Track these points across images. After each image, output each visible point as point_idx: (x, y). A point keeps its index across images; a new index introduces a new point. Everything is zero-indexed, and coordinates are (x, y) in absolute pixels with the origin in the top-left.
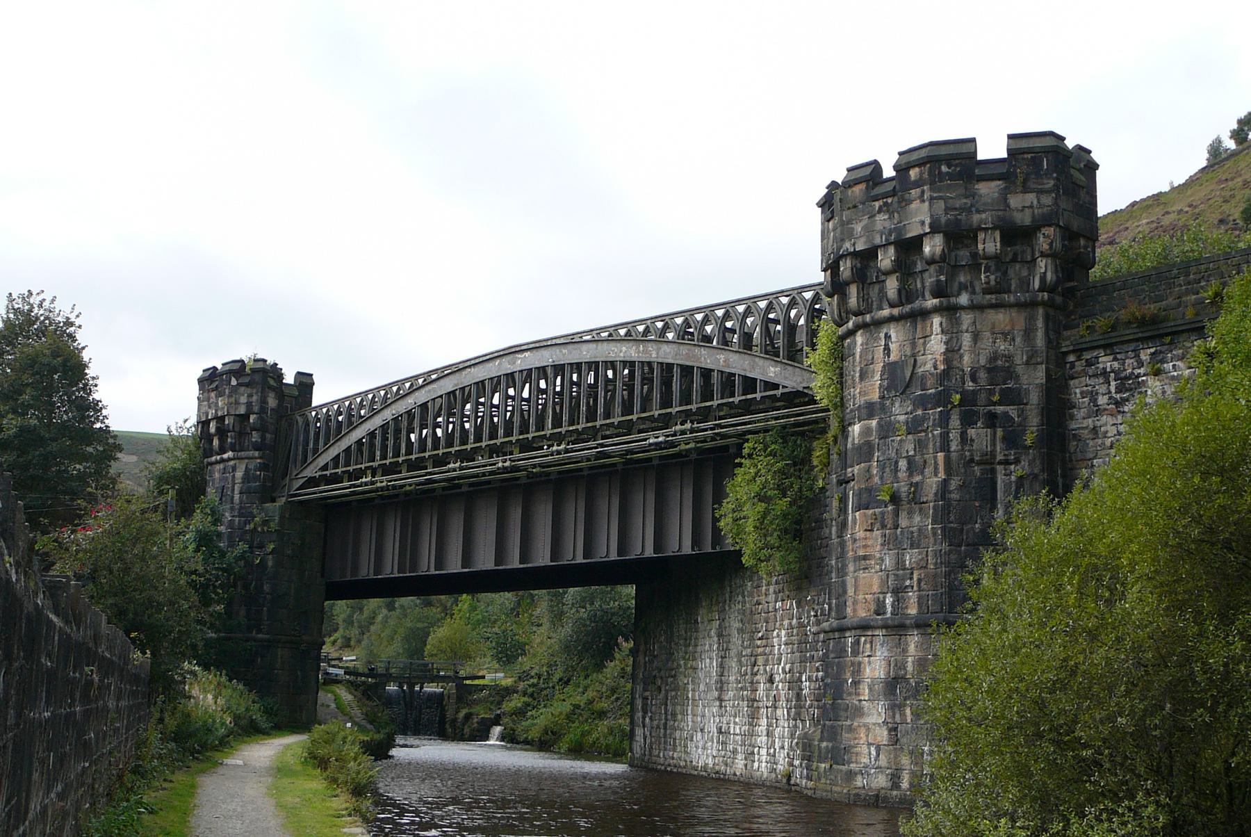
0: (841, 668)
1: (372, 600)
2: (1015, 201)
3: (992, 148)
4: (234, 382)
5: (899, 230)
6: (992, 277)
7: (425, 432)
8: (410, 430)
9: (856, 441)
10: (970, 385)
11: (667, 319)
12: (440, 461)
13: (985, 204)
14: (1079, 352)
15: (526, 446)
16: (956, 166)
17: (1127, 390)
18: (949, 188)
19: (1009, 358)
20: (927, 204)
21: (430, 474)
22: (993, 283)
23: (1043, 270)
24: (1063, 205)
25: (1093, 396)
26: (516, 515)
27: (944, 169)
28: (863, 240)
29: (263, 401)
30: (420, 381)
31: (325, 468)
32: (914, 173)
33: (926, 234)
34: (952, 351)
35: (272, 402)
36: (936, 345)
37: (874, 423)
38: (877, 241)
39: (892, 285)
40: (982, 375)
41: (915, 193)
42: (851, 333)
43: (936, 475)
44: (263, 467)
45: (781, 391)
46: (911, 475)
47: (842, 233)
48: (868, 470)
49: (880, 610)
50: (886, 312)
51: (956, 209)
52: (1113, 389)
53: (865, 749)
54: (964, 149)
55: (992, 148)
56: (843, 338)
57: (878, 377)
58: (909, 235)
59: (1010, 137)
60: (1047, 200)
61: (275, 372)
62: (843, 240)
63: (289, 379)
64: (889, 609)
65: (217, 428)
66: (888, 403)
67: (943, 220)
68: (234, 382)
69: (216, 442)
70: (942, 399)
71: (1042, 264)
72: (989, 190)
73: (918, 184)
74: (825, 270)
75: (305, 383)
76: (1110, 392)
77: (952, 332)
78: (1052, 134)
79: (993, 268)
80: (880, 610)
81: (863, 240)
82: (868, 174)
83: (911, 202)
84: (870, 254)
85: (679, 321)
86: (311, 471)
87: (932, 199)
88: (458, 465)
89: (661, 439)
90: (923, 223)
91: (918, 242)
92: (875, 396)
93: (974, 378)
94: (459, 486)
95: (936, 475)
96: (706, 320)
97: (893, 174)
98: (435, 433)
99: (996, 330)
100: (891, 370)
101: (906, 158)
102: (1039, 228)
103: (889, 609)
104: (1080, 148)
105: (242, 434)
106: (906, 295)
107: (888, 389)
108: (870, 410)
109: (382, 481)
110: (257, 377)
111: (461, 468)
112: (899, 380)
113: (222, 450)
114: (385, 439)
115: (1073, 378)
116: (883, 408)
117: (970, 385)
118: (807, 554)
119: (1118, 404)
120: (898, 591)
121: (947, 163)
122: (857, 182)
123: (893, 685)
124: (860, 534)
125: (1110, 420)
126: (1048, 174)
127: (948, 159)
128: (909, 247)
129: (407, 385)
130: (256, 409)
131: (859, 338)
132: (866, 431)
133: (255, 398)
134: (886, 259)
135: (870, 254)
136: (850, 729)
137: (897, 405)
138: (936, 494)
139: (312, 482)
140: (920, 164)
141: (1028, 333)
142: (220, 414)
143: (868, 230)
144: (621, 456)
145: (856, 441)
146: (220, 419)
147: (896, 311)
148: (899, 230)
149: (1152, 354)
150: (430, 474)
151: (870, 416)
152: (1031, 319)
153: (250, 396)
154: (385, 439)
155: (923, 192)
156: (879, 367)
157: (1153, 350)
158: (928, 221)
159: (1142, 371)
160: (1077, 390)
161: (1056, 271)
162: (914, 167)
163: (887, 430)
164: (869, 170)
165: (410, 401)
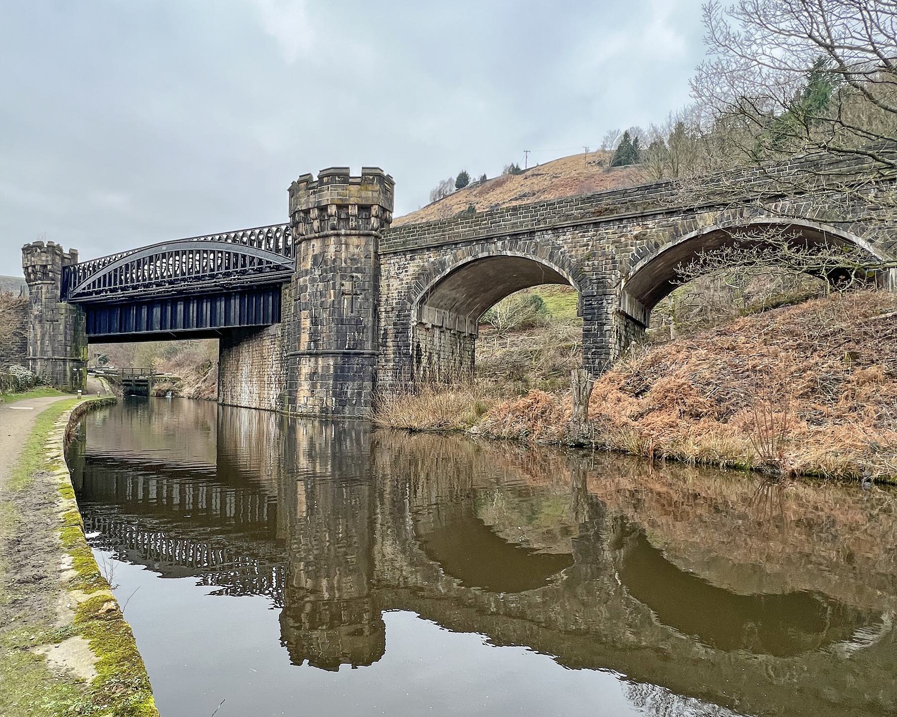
2: (363, 194)
4: (39, 250)
31: (84, 289)
32: (325, 179)
36: (332, 249)
37: (307, 278)
39: (316, 224)
40: (349, 261)
42: (300, 243)
50: (313, 235)
54: (344, 171)
55: (356, 172)
60: (376, 194)
63: (66, 251)
68: (39, 250)
69: (32, 276)
70: (333, 270)
71: (373, 219)
72: (354, 188)
73: (327, 183)
75: (74, 254)
82: (306, 180)
84: (307, 212)
86: (79, 290)
92: (309, 267)
100: (315, 258)
102: (372, 205)
104: (388, 175)
105: (45, 274)
108: (307, 272)
110: (50, 249)
113: (35, 280)
114: (115, 276)
116: (311, 273)
121: (338, 176)
122: (302, 182)
123: (312, 375)
127: (339, 175)
128: (323, 209)
131: (303, 245)
132: (305, 281)
133: (49, 258)
134: (314, 213)
135: (307, 212)
139: (79, 295)
140: (327, 176)
143: (307, 202)
146: (34, 266)
147: (317, 235)
154: (115, 276)
163: (313, 280)
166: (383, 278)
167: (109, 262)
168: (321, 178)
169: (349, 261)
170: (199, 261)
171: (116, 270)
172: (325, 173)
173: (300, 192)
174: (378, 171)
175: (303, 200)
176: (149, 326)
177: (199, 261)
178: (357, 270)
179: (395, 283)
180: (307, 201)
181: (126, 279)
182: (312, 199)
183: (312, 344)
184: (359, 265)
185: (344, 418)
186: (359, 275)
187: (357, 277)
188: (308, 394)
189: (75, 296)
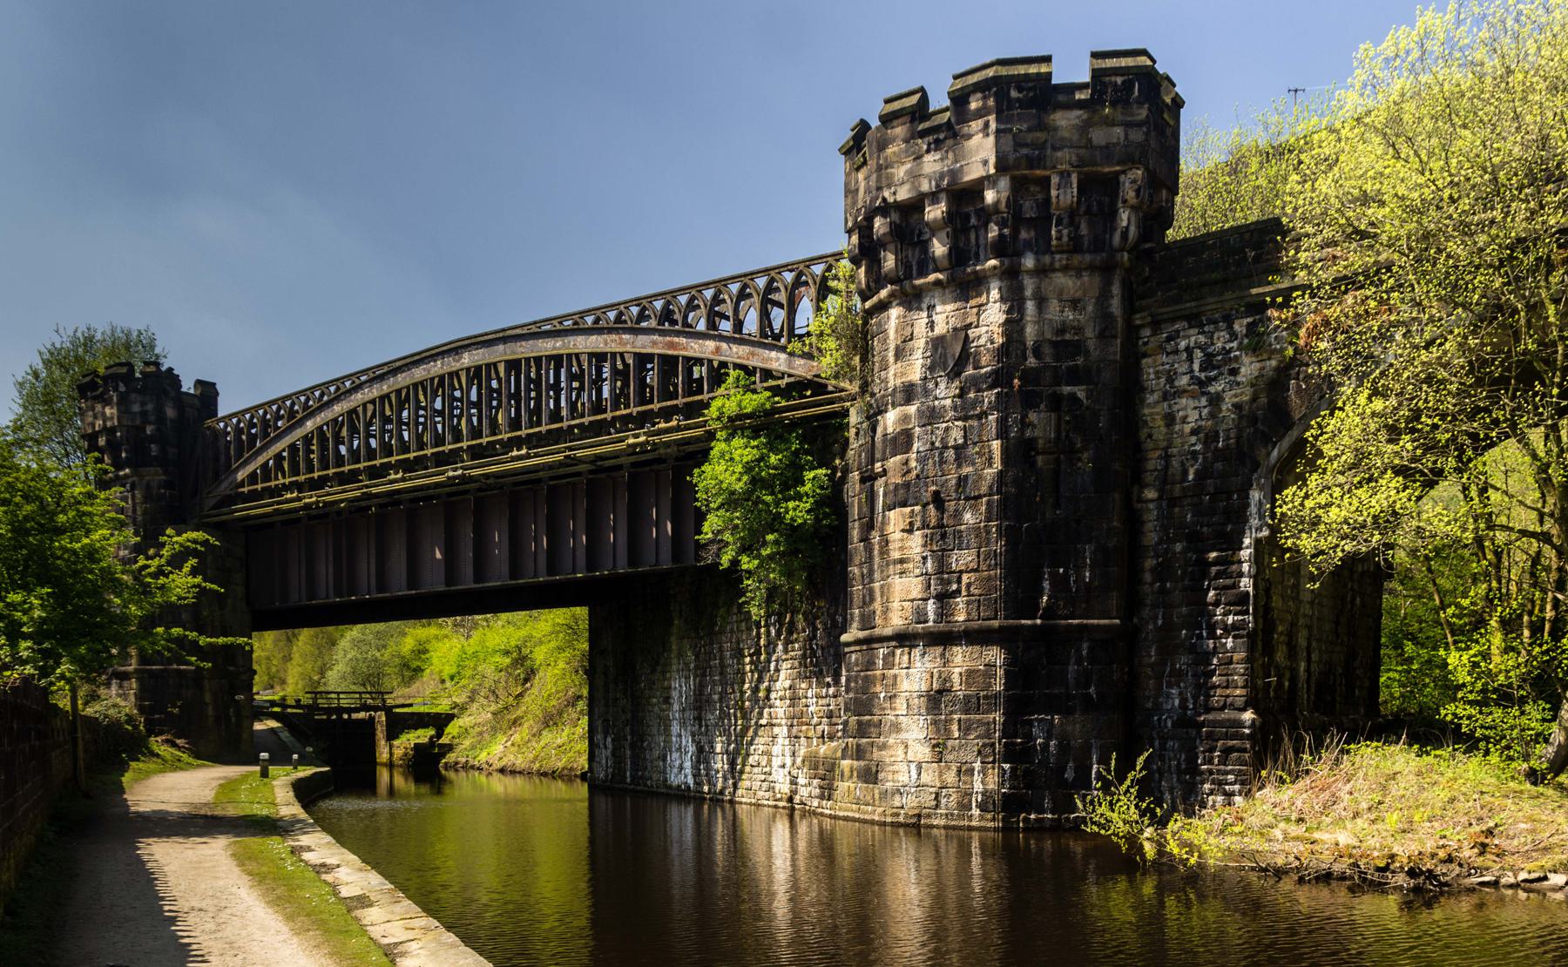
0: (869, 681)
1: (1182, 166)
3: (1072, 69)
5: (954, 174)
6: (1065, 232)
7: (356, 443)
8: (339, 441)
9: (890, 430)
10: (1032, 361)
11: (643, 303)
12: (377, 473)
13: (1063, 139)
14: (1156, 326)
15: (477, 453)
16: (1030, 89)
17: (1214, 368)
18: (1020, 119)
19: (1079, 329)
20: (992, 139)
21: (367, 487)
22: (1065, 239)
23: (1125, 224)
24: (1153, 143)
25: (1171, 377)
26: (467, 534)
27: (1014, 94)
28: (906, 187)
29: (160, 411)
30: (348, 384)
33: (988, 177)
34: (1013, 327)
35: (170, 413)
37: (912, 409)
38: (925, 187)
40: (1047, 350)
41: (976, 125)
42: (883, 306)
43: (990, 466)
44: (168, 485)
45: (787, 380)
46: (959, 466)
47: (879, 180)
48: (907, 462)
49: (921, 617)
51: (1026, 145)
52: (1196, 367)
53: (903, 767)
55: (1072, 69)
56: (868, 313)
57: (918, 354)
58: (967, 178)
59: (1095, 55)
61: (172, 378)
62: (879, 189)
63: (188, 386)
64: (931, 616)
65: (108, 441)
66: (931, 385)
67: (1012, 158)
73: (980, 114)
74: (849, 232)
75: (208, 392)
76: (1192, 371)
77: (1013, 300)
78: (1144, 52)
79: (1066, 221)
80: (921, 617)
81: (906, 187)
83: (970, 137)
84: (915, 206)
85: (659, 305)
87: (998, 131)
88: (400, 476)
89: (642, 439)
90: (985, 163)
91: (977, 188)
93: (1037, 352)
94: (399, 503)
95: (990, 466)
96: (691, 306)
97: (947, 103)
98: (368, 444)
99: (1065, 297)
100: (937, 344)
101: (959, 84)
103: (931, 616)
106: (959, 256)
107: (931, 368)
108: (909, 393)
109: (310, 498)
111: (403, 479)
112: (952, 356)
115: (1145, 355)
116: (926, 392)
117: (1032, 361)
118: (822, 567)
119: (1202, 384)
120: (944, 598)
123: (936, 699)
124: (898, 535)
125: (1192, 403)
126: (1140, 103)
127: (1020, 82)
128: (963, 196)
129: (332, 389)
130: (152, 418)
131: (895, 312)
132: (905, 418)
133: (150, 407)
134: (934, 212)
136: (884, 747)
137: (942, 386)
138: (991, 487)
140: (982, 87)
141: (1104, 296)
142: (109, 424)
143: (914, 176)
144: (592, 462)
145: (890, 430)
148: (954, 174)
149: (1249, 325)
150: (367, 487)
151: (908, 401)
152: (1106, 285)
153: (143, 404)
155: (987, 125)
156: (920, 344)
157: (1250, 320)
158: (992, 160)
159: (1235, 344)
160: (1151, 370)
161: (1138, 227)
162: (974, 92)
163: (931, 416)
164: (915, 99)
165: (338, 408)
166: (1151, 399)
167: (306, 406)
168: (959, 99)
169: (1047, 350)
170: (478, 405)
171: (307, 440)
172: (896, 105)
173: (890, 150)
174: (1143, 61)
175: (900, 172)
176: (413, 579)
177: (478, 405)
178: (1075, 377)
179: (1191, 412)
180: (913, 172)
181: (309, 463)
182: (932, 163)
183: (931, 606)
184: (1080, 361)
185: (970, 829)
186: (1080, 392)
187: (1073, 396)
188: (922, 752)
189: (215, 507)
